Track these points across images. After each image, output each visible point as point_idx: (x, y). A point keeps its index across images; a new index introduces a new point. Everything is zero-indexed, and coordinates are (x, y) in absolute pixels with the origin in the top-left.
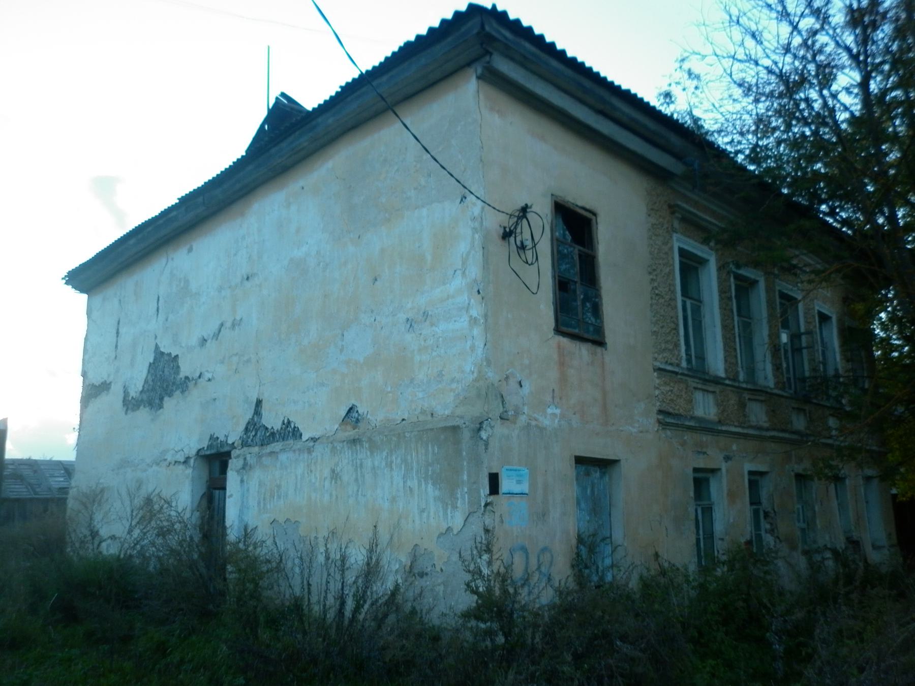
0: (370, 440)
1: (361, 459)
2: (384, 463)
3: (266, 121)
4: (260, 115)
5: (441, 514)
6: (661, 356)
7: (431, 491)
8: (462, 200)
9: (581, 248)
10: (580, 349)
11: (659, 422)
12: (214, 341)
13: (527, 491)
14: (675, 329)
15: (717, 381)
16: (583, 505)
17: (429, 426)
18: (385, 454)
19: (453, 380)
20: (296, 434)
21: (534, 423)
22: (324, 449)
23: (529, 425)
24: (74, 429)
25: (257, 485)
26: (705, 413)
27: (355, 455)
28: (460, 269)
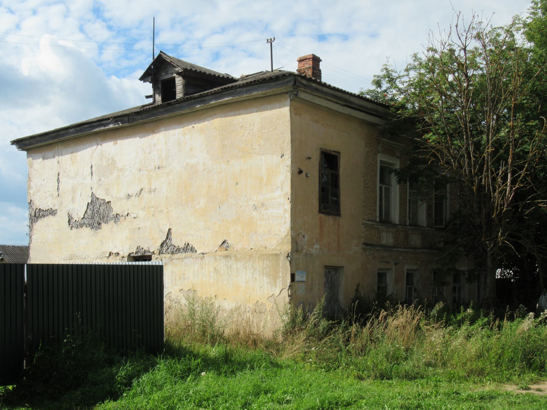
0: (235, 256)
1: (231, 264)
2: (242, 267)
3: (152, 64)
4: (150, 61)
5: (270, 289)
6: (366, 217)
7: (265, 280)
8: (282, 156)
9: (332, 171)
10: (329, 218)
11: (363, 248)
12: (137, 197)
13: (305, 281)
14: (375, 203)
15: (395, 225)
16: (327, 285)
17: (265, 253)
18: (243, 263)
19: (276, 235)
20: (193, 250)
21: (308, 253)
22: (210, 259)
23: (307, 253)
24: (27, 234)
25: (171, 273)
26: (387, 242)
27: (227, 262)
28: (280, 187)
